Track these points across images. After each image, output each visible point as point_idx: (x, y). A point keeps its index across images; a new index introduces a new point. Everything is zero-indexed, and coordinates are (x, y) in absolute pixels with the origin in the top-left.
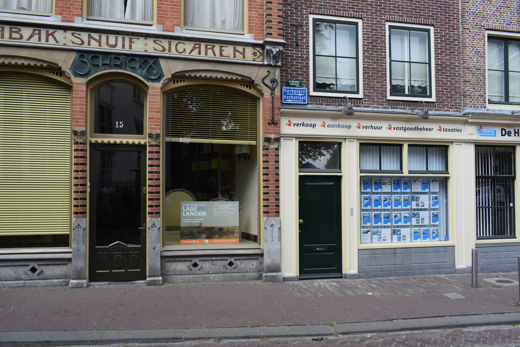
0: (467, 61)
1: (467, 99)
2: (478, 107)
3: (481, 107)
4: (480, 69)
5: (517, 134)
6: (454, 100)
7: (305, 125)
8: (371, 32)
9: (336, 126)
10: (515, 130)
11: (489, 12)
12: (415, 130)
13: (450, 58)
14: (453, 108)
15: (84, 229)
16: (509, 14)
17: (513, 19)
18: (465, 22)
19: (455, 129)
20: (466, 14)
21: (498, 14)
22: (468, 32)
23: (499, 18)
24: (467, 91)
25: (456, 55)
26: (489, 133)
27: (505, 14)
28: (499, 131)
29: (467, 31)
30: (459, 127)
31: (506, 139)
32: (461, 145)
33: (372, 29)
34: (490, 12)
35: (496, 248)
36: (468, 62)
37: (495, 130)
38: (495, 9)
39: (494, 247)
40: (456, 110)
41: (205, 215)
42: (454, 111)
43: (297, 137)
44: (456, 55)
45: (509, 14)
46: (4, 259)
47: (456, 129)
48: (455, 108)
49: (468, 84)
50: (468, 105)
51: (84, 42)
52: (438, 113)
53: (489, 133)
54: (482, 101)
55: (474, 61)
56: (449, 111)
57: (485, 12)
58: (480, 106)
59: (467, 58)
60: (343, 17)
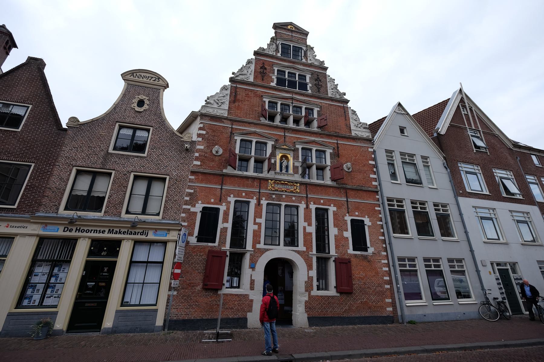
0: (50, 184)
1: (42, 207)
3: (52, 212)
5: (77, 231)
7: (122, 233)
9: (96, 231)
10: (77, 228)
12: (143, 235)
18: (58, 162)
19: (21, 226)
20: (60, 157)
23: (87, 160)
24: (44, 202)
26: (52, 230)
28: (61, 228)
30: (25, 225)
31: (68, 234)
32: (25, 237)
35: (29, 316)
36: (51, 184)
37: (58, 227)
39: (26, 316)
40: (31, 214)
43: (37, 235)
47: (22, 226)
50: (40, 211)
51: (235, 201)
52: (13, 215)
53: (52, 230)
54: (54, 209)
55: (57, 184)
56: (25, 214)
58: (51, 212)
59: (51, 182)
60: (96, 168)
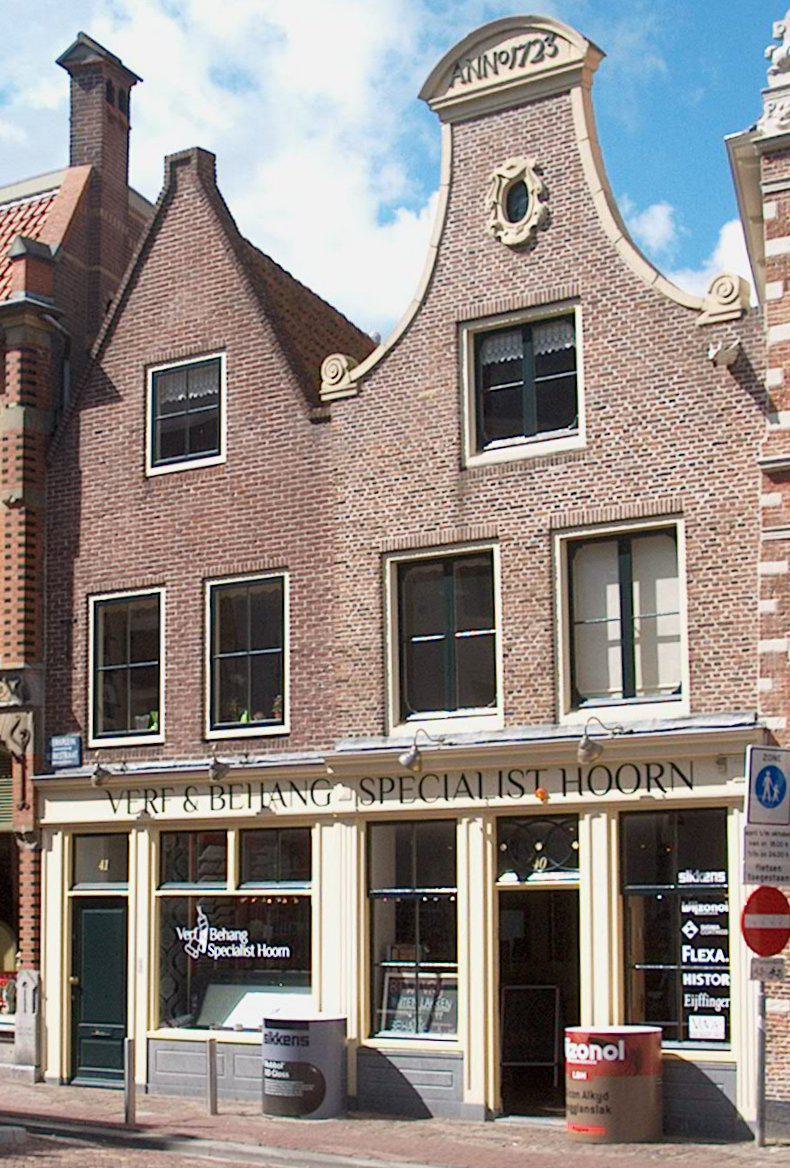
2: (365, 735)
3: (357, 736)
4: (369, 649)
6: (324, 726)
8: (178, 607)
11: (387, 513)
13: (317, 631)
14: (320, 743)
15: (605, 1151)
16: (432, 503)
17: (441, 515)
21: (409, 510)
22: (344, 569)
25: (329, 624)
27: (424, 507)
29: (342, 567)
33: (179, 602)
34: (391, 511)
38: (402, 501)
41: (622, 1057)
42: (323, 749)
44: (329, 624)
45: (432, 503)
46: (29, 1112)
48: (326, 743)
49: (344, 686)
56: (313, 750)
57: (380, 515)
58: (369, 733)
